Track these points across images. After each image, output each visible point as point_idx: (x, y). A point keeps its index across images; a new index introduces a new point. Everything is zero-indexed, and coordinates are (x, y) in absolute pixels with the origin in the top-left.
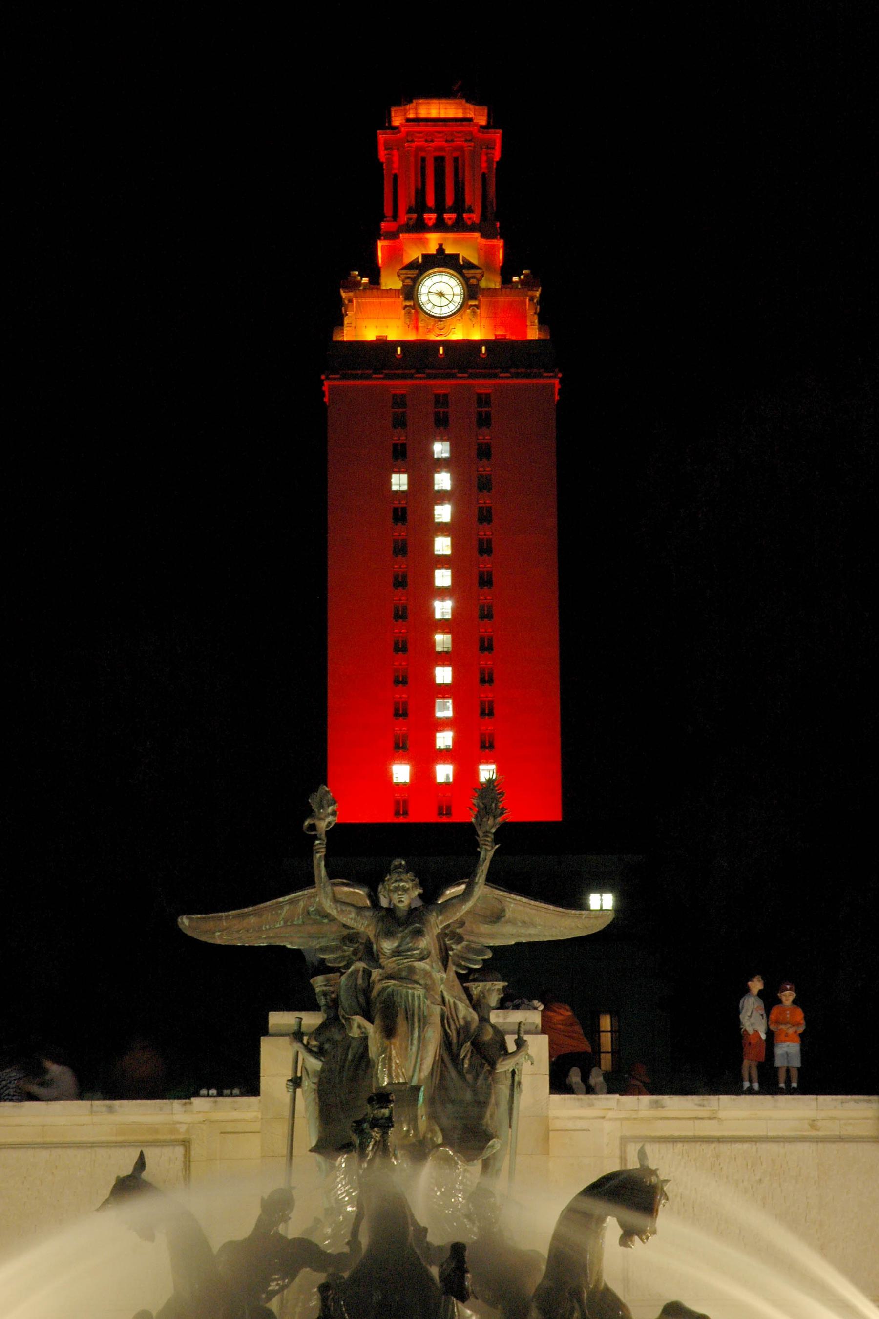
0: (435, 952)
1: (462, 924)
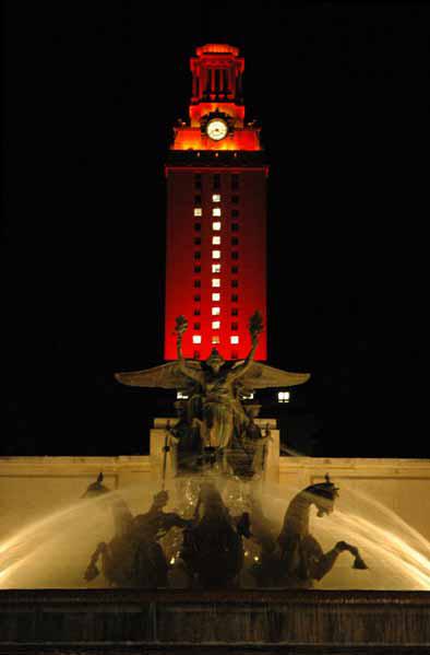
0: (230, 389)
1: (242, 378)
